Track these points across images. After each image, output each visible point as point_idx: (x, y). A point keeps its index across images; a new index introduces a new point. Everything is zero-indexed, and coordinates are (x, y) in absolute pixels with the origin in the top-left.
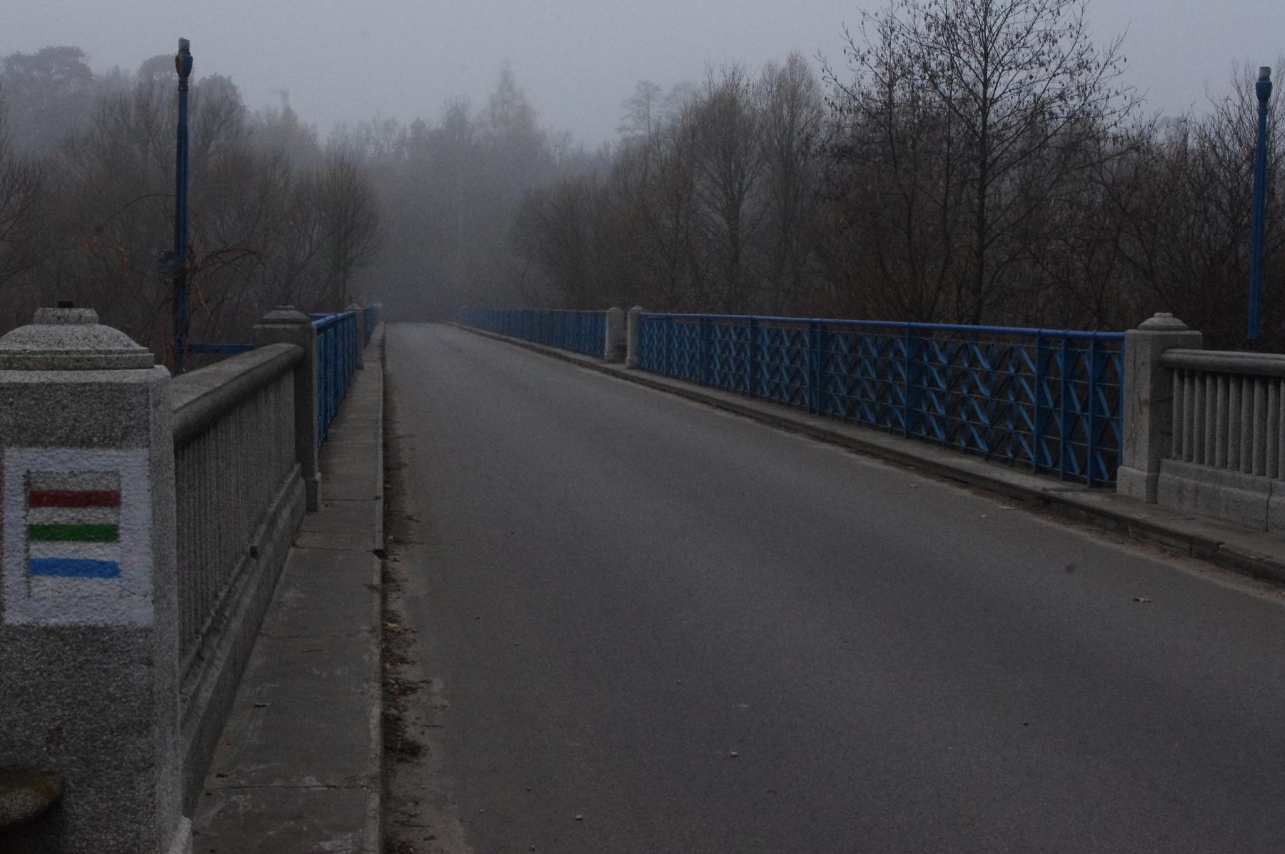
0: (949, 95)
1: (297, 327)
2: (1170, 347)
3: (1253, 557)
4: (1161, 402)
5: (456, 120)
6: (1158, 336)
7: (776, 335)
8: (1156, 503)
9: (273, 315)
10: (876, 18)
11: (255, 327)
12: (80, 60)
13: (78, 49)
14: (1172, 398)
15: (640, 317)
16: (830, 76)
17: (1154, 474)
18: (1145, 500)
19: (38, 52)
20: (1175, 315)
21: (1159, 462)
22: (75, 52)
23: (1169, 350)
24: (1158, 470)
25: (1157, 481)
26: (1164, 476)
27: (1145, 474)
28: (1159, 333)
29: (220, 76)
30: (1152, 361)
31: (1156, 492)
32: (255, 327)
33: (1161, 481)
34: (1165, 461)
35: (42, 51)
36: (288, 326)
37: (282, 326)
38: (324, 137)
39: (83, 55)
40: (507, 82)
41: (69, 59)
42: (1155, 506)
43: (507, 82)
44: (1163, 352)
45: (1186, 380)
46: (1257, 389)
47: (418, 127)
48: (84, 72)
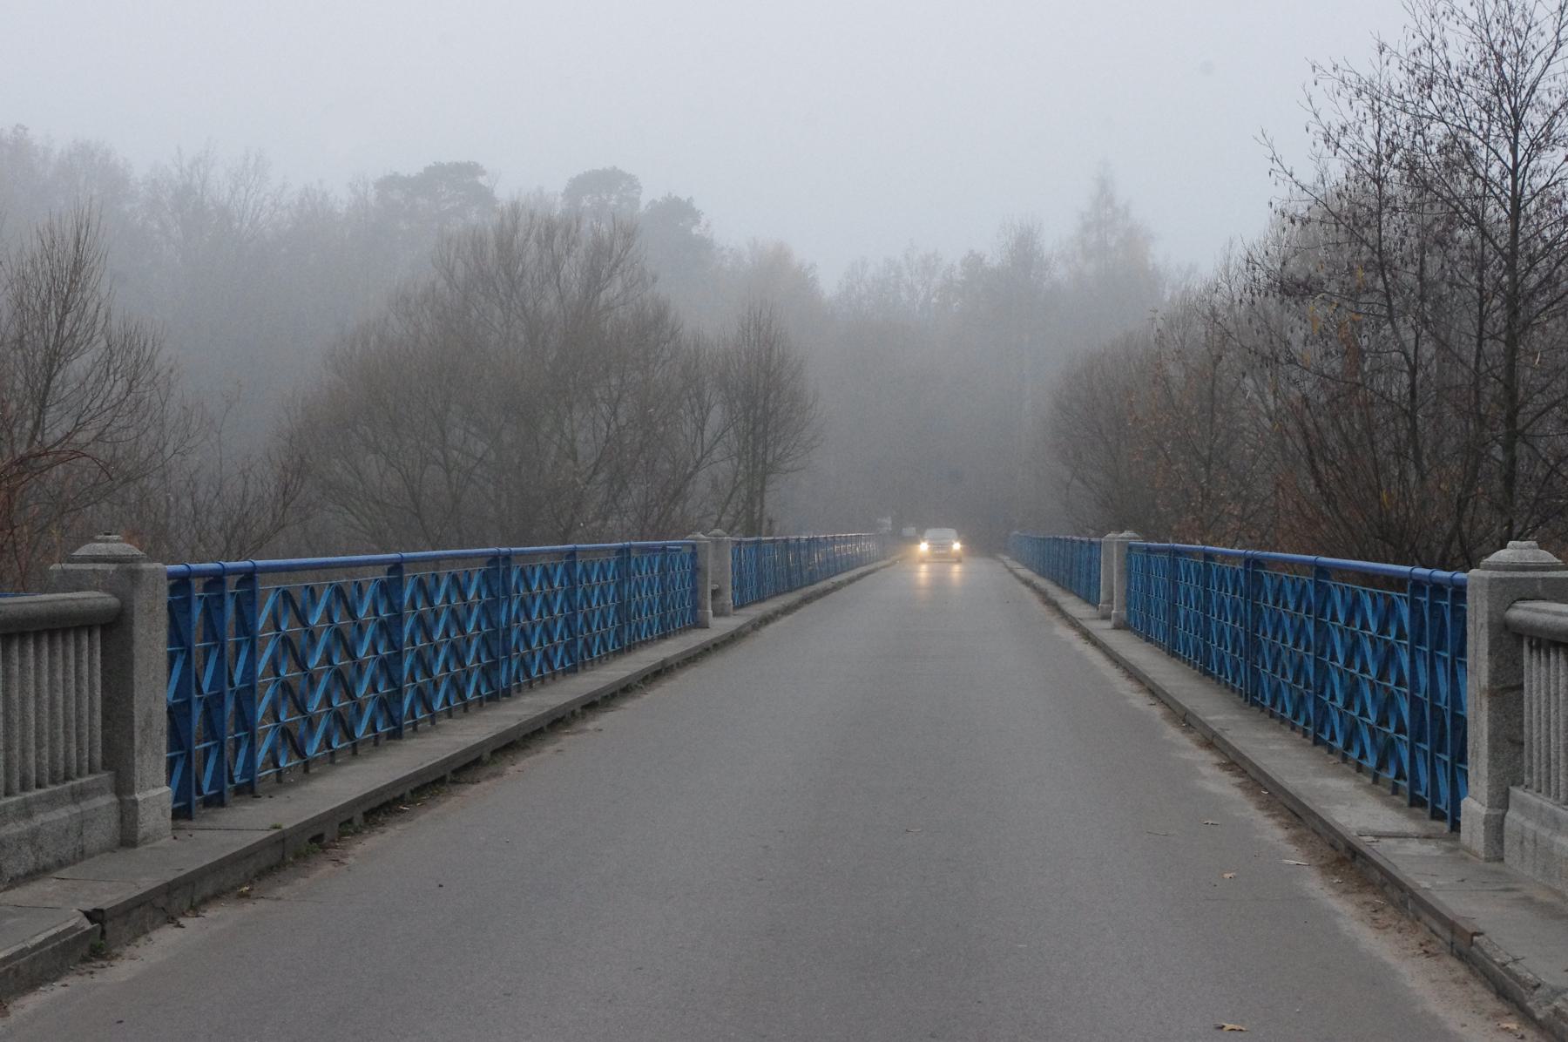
0: (1481, 191)
1: (113, 567)
2: (1523, 599)
3: (1497, 960)
4: (1507, 690)
5: (1025, 251)
6: (1502, 580)
7: (1205, 575)
8: (1502, 860)
9: (83, 551)
10: (1336, 75)
11: (51, 568)
12: (482, 180)
13: (476, 165)
14: (1522, 685)
15: (1130, 548)
16: (1280, 169)
17: (1500, 812)
18: (1483, 855)
19: (422, 171)
20: (1543, 544)
21: (1507, 793)
22: (473, 169)
23: (1519, 604)
24: (1505, 805)
25: (1502, 825)
26: (1513, 815)
27: (139, 797)
28: (1508, 575)
29: (676, 197)
30: (1491, 625)
31: (1501, 842)
32: (51, 568)
33: (1507, 822)
34: (1516, 792)
35: (428, 169)
36: (99, 566)
37: (90, 566)
38: (829, 283)
39: (483, 173)
40: (1104, 194)
41: (462, 177)
42: (1495, 866)
43: (1104, 194)
44: (1509, 607)
45: (1534, 654)
46: (72, 638)
47: (974, 263)
48: (484, 197)
